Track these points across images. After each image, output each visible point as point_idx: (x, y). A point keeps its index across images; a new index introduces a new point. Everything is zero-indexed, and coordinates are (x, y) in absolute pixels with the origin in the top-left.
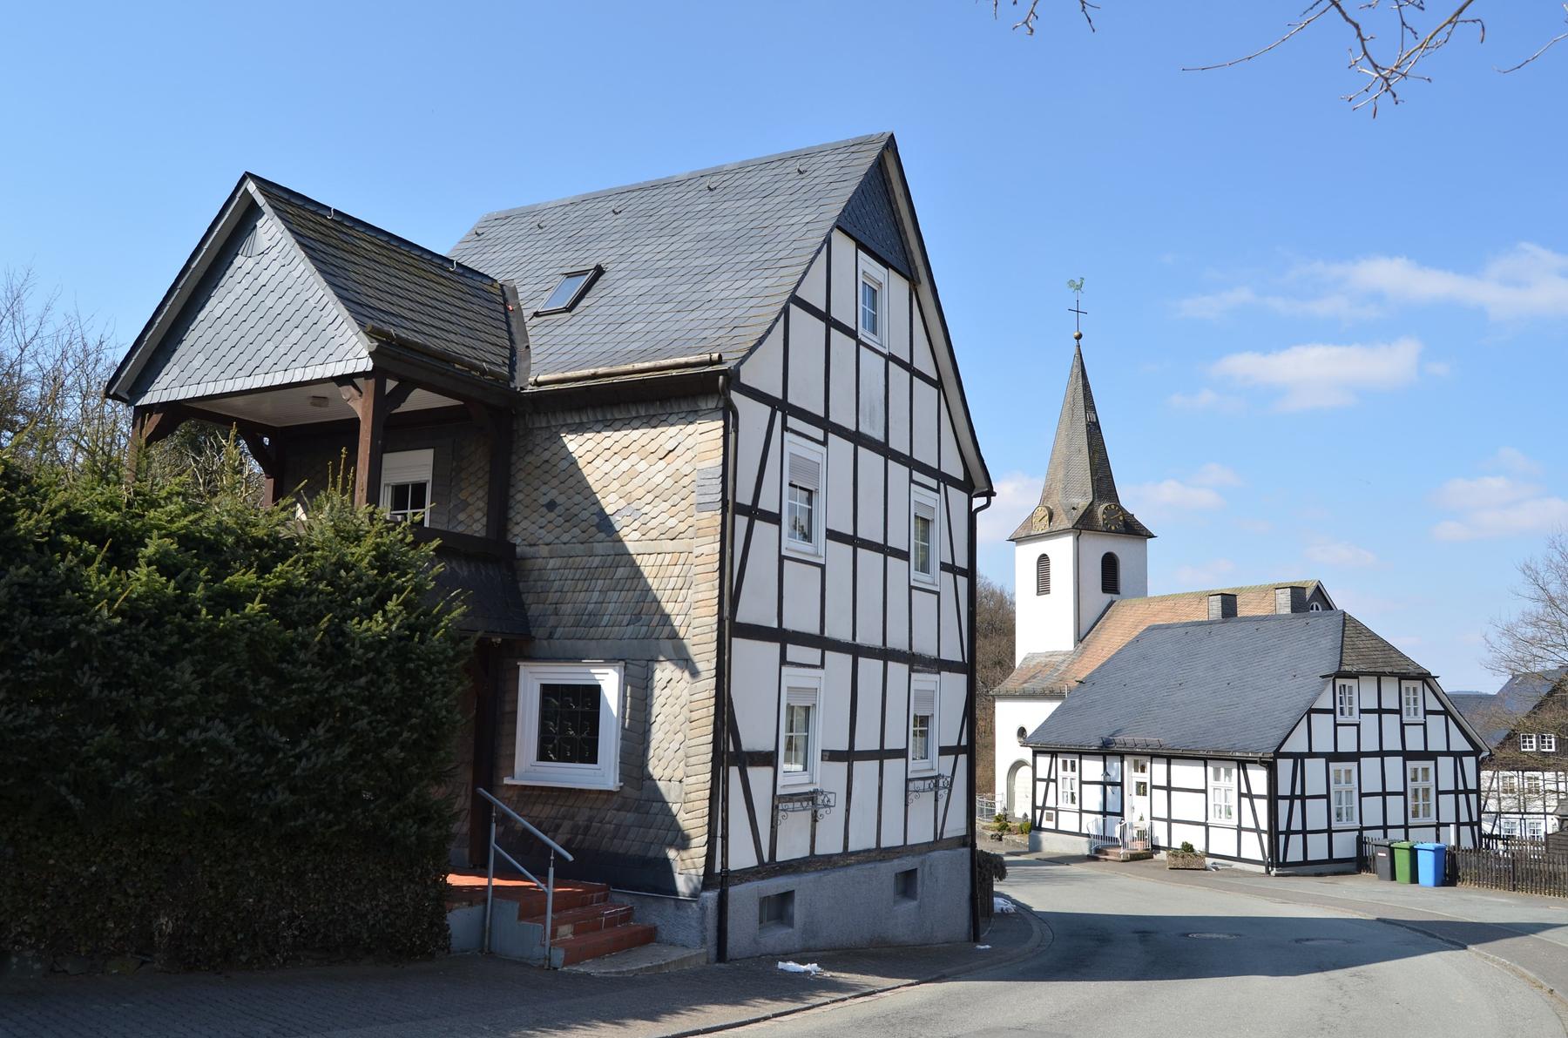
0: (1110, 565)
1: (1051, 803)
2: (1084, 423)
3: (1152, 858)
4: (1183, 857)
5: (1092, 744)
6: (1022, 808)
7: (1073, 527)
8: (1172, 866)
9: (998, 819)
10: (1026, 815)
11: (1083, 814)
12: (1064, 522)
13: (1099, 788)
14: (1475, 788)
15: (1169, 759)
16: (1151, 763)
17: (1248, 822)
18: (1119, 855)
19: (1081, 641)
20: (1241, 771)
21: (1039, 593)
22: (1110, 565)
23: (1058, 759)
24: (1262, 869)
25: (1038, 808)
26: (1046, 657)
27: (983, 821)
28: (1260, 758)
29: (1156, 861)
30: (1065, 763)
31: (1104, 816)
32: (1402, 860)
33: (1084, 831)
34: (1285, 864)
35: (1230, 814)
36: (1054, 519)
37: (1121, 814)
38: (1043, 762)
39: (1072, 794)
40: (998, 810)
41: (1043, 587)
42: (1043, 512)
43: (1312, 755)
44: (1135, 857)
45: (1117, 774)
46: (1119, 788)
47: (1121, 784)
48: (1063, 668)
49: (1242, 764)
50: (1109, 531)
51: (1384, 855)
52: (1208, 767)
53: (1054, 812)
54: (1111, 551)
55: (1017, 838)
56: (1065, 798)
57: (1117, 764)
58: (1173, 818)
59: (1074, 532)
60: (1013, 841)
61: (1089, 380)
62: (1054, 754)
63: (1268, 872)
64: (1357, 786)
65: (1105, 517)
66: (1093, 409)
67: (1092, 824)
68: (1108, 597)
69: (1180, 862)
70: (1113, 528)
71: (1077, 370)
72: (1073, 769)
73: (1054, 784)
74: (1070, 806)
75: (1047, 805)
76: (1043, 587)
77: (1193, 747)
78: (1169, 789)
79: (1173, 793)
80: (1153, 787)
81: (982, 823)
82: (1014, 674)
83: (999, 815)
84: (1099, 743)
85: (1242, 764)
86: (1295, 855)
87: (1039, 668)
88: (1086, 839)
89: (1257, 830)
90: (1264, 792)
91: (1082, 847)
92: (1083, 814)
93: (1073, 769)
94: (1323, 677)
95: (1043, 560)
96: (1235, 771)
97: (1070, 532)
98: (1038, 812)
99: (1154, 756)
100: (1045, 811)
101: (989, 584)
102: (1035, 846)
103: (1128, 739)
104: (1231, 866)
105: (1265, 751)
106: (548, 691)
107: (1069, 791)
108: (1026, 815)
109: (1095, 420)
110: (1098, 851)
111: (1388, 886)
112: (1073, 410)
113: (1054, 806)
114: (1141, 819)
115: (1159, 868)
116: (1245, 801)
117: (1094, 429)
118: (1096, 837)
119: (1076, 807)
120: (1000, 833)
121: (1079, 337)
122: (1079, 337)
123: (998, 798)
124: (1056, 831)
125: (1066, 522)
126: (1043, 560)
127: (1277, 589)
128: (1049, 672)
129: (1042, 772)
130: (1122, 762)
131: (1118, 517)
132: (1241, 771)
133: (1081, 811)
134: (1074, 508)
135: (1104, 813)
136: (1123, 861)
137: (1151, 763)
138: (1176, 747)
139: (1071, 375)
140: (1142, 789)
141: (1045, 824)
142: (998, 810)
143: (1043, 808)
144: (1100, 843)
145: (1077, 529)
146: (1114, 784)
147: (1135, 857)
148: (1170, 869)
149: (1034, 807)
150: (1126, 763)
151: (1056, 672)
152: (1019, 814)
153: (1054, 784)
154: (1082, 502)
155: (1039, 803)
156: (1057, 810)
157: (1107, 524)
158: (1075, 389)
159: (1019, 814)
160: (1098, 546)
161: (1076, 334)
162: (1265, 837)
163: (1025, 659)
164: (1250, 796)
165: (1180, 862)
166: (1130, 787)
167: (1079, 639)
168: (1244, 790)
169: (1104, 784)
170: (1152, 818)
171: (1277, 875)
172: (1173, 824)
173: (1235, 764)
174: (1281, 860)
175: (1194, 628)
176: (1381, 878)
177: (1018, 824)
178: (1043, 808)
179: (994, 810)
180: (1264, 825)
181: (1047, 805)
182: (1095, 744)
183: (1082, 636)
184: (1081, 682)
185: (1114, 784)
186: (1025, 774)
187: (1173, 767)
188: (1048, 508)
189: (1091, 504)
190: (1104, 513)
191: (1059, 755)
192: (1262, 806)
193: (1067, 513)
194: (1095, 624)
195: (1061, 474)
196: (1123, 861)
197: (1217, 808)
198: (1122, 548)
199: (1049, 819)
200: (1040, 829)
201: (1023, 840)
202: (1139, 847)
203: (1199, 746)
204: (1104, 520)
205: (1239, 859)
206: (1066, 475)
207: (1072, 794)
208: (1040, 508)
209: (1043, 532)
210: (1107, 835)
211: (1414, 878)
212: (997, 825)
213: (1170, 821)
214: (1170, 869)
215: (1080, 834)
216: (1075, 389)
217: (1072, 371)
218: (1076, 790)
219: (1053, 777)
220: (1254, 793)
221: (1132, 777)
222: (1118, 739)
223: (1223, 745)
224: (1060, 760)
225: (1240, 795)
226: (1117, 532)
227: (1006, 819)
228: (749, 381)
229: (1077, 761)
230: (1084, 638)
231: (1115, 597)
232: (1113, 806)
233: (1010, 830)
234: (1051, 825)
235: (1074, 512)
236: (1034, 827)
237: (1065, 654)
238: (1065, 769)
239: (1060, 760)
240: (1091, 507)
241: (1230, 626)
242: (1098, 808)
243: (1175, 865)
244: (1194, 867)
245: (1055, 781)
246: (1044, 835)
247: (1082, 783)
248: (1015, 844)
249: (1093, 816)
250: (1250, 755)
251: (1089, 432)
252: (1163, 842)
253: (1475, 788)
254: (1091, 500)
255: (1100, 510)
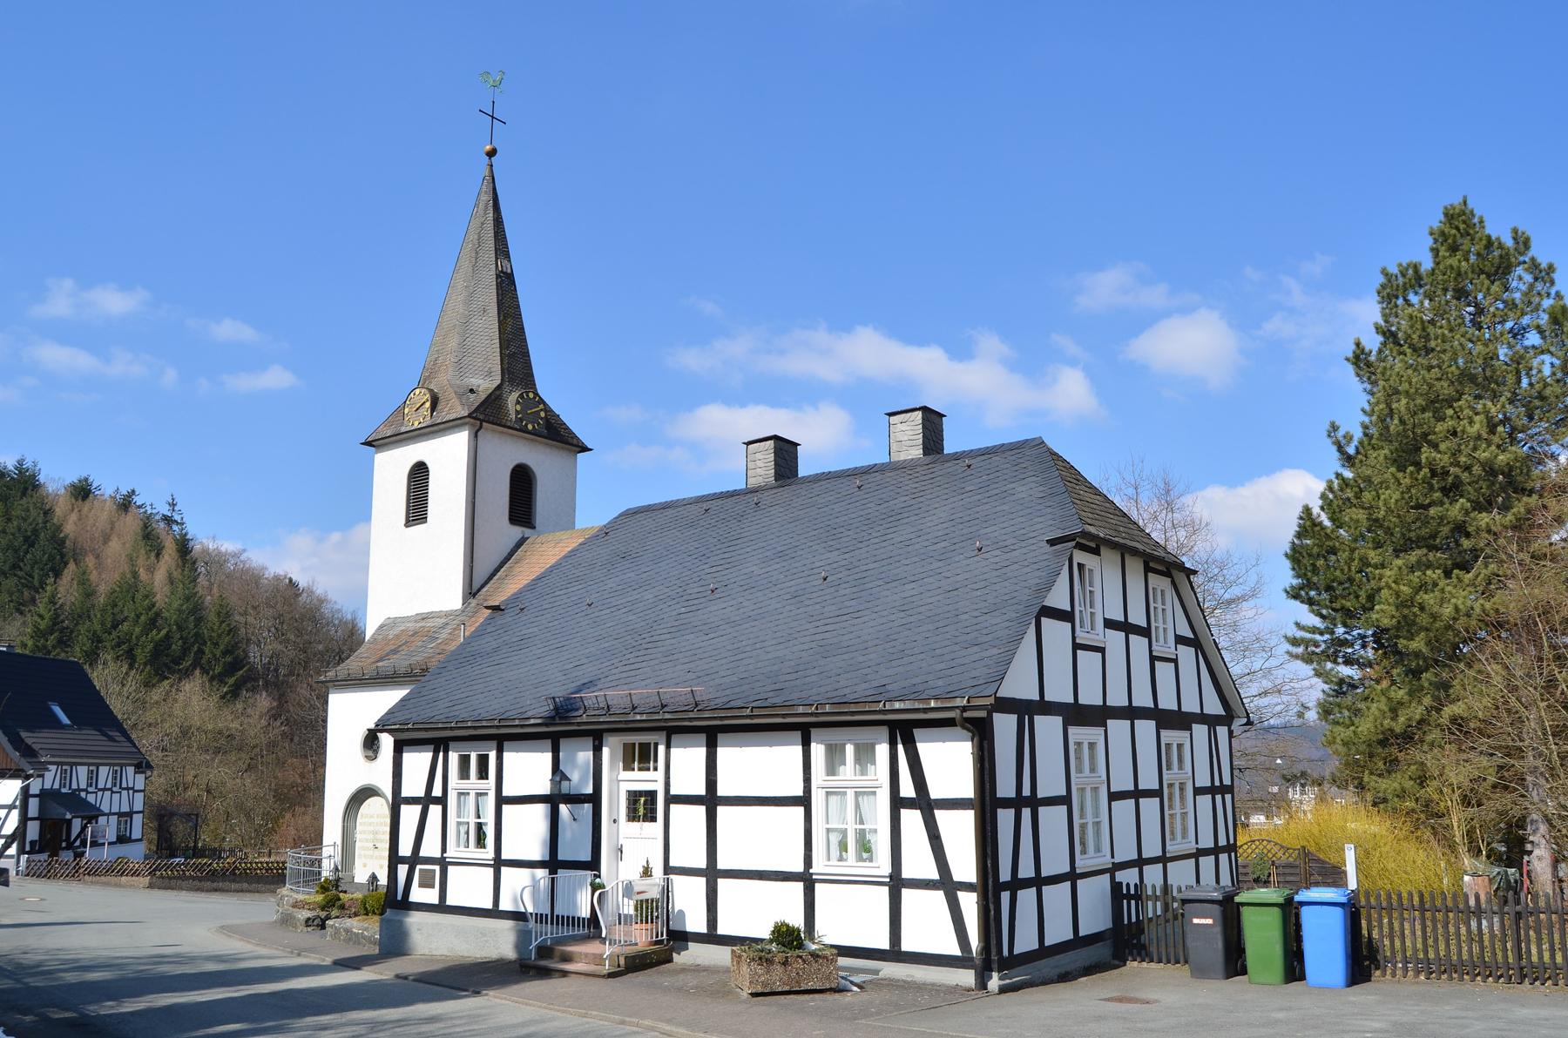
0: (522, 482)
1: (430, 848)
2: (493, 272)
3: (670, 960)
4: (785, 963)
5: (529, 714)
6: (370, 865)
7: (470, 416)
8: (760, 989)
9: (324, 888)
10: (374, 878)
11: (504, 870)
12: (455, 408)
13: (540, 811)
14: (903, 812)
15: (712, 736)
16: (668, 747)
17: (917, 862)
18: (599, 959)
19: (474, 595)
20: (900, 748)
21: (408, 523)
22: (522, 482)
23: (451, 754)
24: (967, 977)
25: (403, 860)
26: (416, 621)
27: (298, 892)
28: (964, 709)
29: (684, 970)
30: (464, 762)
31: (553, 871)
32: (1262, 932)
33: (506, 905)
34: (1012, 962)
35: (869, 850)
36: (439, 407)
37: (594, 864)
38: (417, 763)
39: (480, 827)
40: (326, 872)
41: (417, 511)
42: (422, 396)
43: (1045, 707)
44: (636, 964)
45: (583, 780)
46: (588, 807)
47: (595, 799)
48: (444, 635)
49: (903, 732)
50: (524, 430)
51: (1209, 921)
52: (813, 745)
53: (437, 868)
54: (524, 462)
55: (355, 924)
56: (463, 836)
57: (585, 756)
58: (722, 864)
59: (472, 425)
60: (347, 931)
61: (503, 214)
62: (440, 745)
63: (982, 984)
64: (1104, 777)
65: (518, 408)
66: (507, 256)
67: (520, 888)
68: (517, 532)
69: (777, 977)
70: (530, 427)
71: (486, 198)
72: (483, 774)
73: (439, 808)
74: (473, 853)
75: (423, 853)
76: (417, 511)
77: (778, 701)
78: (711, 800)
79: (722, 811)
80: (672, 799)
81: (295, 896)
82: (362, 649)
83: (326, 879)
84: (545, 709)
85: (903, 732)
86: (1026, 941)
87: (403, 639)
88: (509, 924)
89: (947, 884)
90: (967, 790)
91: (500, 942)
92: (504, 870)
93: (483, 774)
94: (1052, 542)
95: (419, 473)
96: (882, 750)
97: (466, 424)
98: (403, 870)
99: (674, 731)
100: (437, 868)
101: (339, 611)
102: (394, 944)
103: (617, 696)
104: (876, 972)
105: (972, 692)
106: (420, 870)
107: (473, 821)
108: (374, 878)
109: (509, 271)
110: (545, 951)
111: (1219, 993)
112: (477, 253)
113: (438, 854)
114: (647, 872)
115: (704, 992)
116: (912, 820)
117: (506, 284)
118: (540, 918)
119: (488, 853)
120: (323, 914)
121: (492, 153)
122: (492, 153)
123: (326, 851)
124: (442, 907)
125: (460, 408)
126: (419, 473)
127: (891, 415)
128: (420, 644)
129: (414, 785)
130: (597, 750)
131: (539, 412)
132: (900, 748)
133: (499, 863)
134: (472, 391)
135: (553, 863)
136: (611, 975)
137: (668, 747)
138: (732, 704)
139: (476, 205)
140: (642, 806)
141: (419, 895)
142: (326, 872)
143: (415, 859)
144: (548, 933)
145: (475, 418)
146: (575, 799)
147: (636, 964)
148: (755, 995)
149: (394, 859)
150: (606, 751)
151: (431, 642)
152: (361, 876)
153: (439, 808)
154: (486, 383)
155: (405, 849)
156: (443, 863)
157: (521, 420)
158: (483, 224)
159: (361, 876)
160: (508, 452)
161: (488, 147)
162: (969, 903)
163: (381, 627)
164: (926, 804)
165: (777, 977)
166: (614, 804)
167: (471, 592)
168: (907, 789)
169: (552, 801)
170: (668, 869)
171: (1003, 990)
172: (721, 882)
173: (884, 732)
174: (1006, 952)
175: (720, 502)
176: (1200, 972)
177: (359, 895)
178: (415, 859)
179: (320, 873)
180: (965, 867)
181: (423, 853)
182: (537, 709)
183: (476, 586)
184: (496, 608)
185: (575, 799)
186: (375, 812)
187: (722, 753)
188: (431, 391)
189: (499, 387)
190: (518, 403)
191: (452, 745)
192: (959, 830)
193: (460, 396)
194: (497, 570)
195: (453, 342)
196: (611, 975)
197: (835, 839)
198: (541, 459)
199: (426, 883)
200: (406, 905)
201: (367, 928)
202: (641, 937)
203: (794, 696)
204: (517, 412)
205: (894, 954)
206: (462, 344)
207: (480, 827)
208: (417, 391)
209: (423, 425)
210: (558, 911)
211: (1294, 967)
212: (320, 898)
213: (712, 874)
214: (755, 995)
215: (494, 913)
216: (483, 224)
217: (478, 199)
218: (489, 819)
219: (437, 791)
220: (935, 794)
221: (620, 782)
222: (589, 697)
223: (854, 687)
224: (454, 757)
225: (897, 803)
226: (534, 433)
227: (337, 887)
228: (360, 855)
229: (492, 755)
230: (479, 590)
231: (527, 532)
232: (575, 846)
233: (342, 907)
234: (430, 896)
235: (472, 396)
236: (393, 902)
237: (448, 614)
238: (464, 773)
239: (454, 757)
240: (498, 393)
241: (785, 493)
242: (537, 852)
243: (764, 984)
244: (811, 986)
245: (442, 801)
246: (414, 919)
247: (501, 801)
248: (351, 938)
249: (525, 873)
250: (933, 704)
251: (499, 286)
252: (696, 922)
253: (903, 812)
254: (499, 382)
255: (512, 399)
